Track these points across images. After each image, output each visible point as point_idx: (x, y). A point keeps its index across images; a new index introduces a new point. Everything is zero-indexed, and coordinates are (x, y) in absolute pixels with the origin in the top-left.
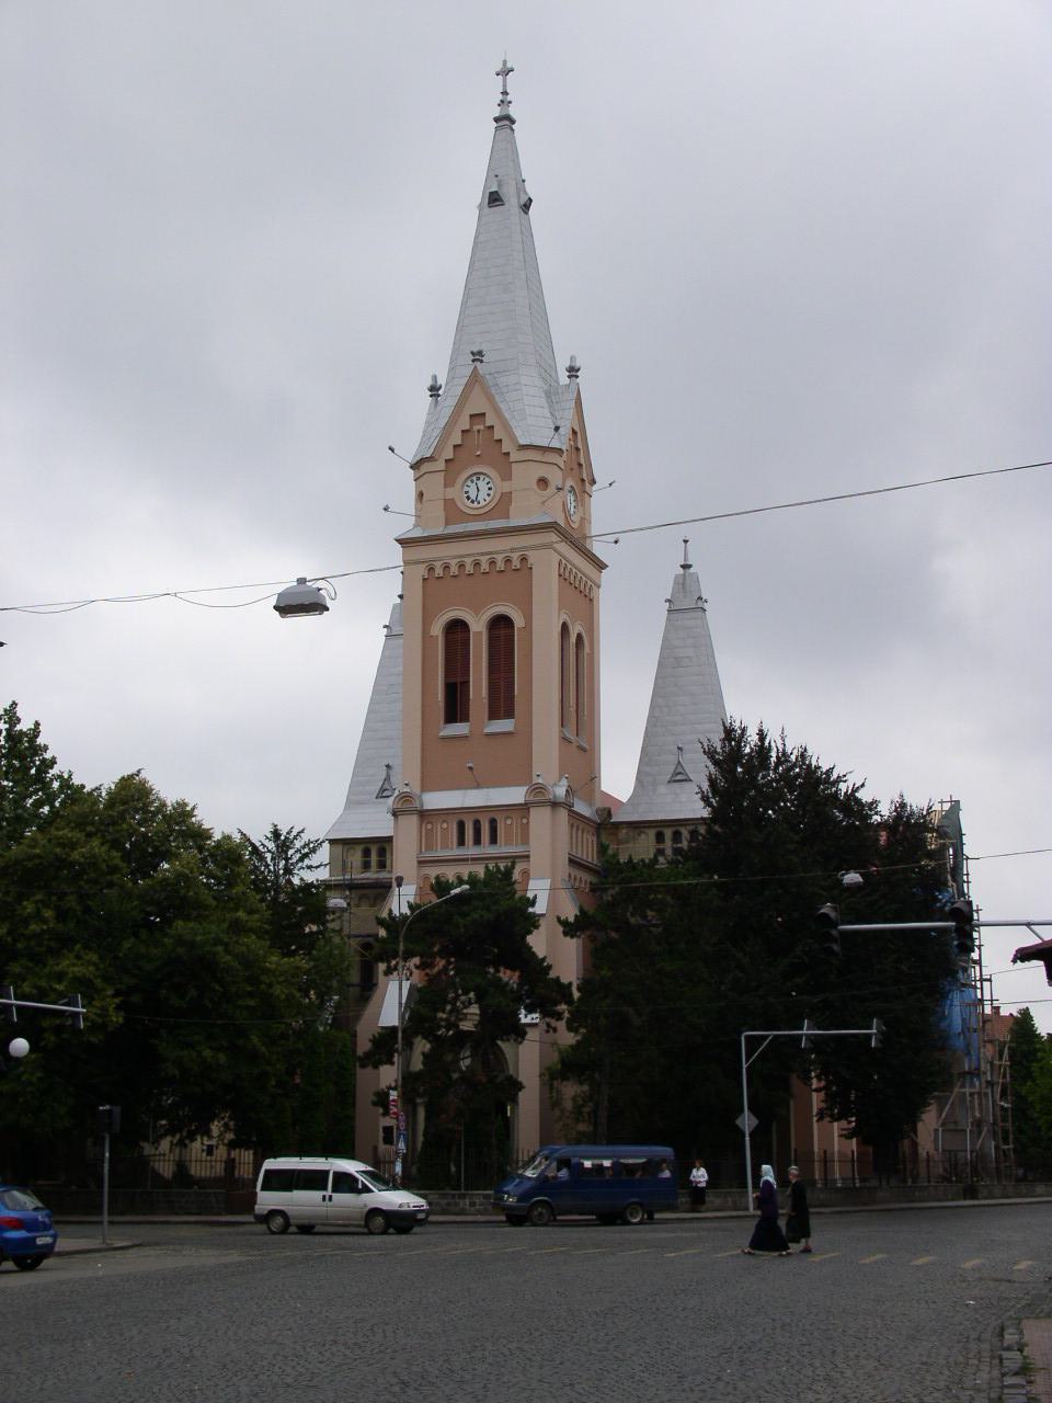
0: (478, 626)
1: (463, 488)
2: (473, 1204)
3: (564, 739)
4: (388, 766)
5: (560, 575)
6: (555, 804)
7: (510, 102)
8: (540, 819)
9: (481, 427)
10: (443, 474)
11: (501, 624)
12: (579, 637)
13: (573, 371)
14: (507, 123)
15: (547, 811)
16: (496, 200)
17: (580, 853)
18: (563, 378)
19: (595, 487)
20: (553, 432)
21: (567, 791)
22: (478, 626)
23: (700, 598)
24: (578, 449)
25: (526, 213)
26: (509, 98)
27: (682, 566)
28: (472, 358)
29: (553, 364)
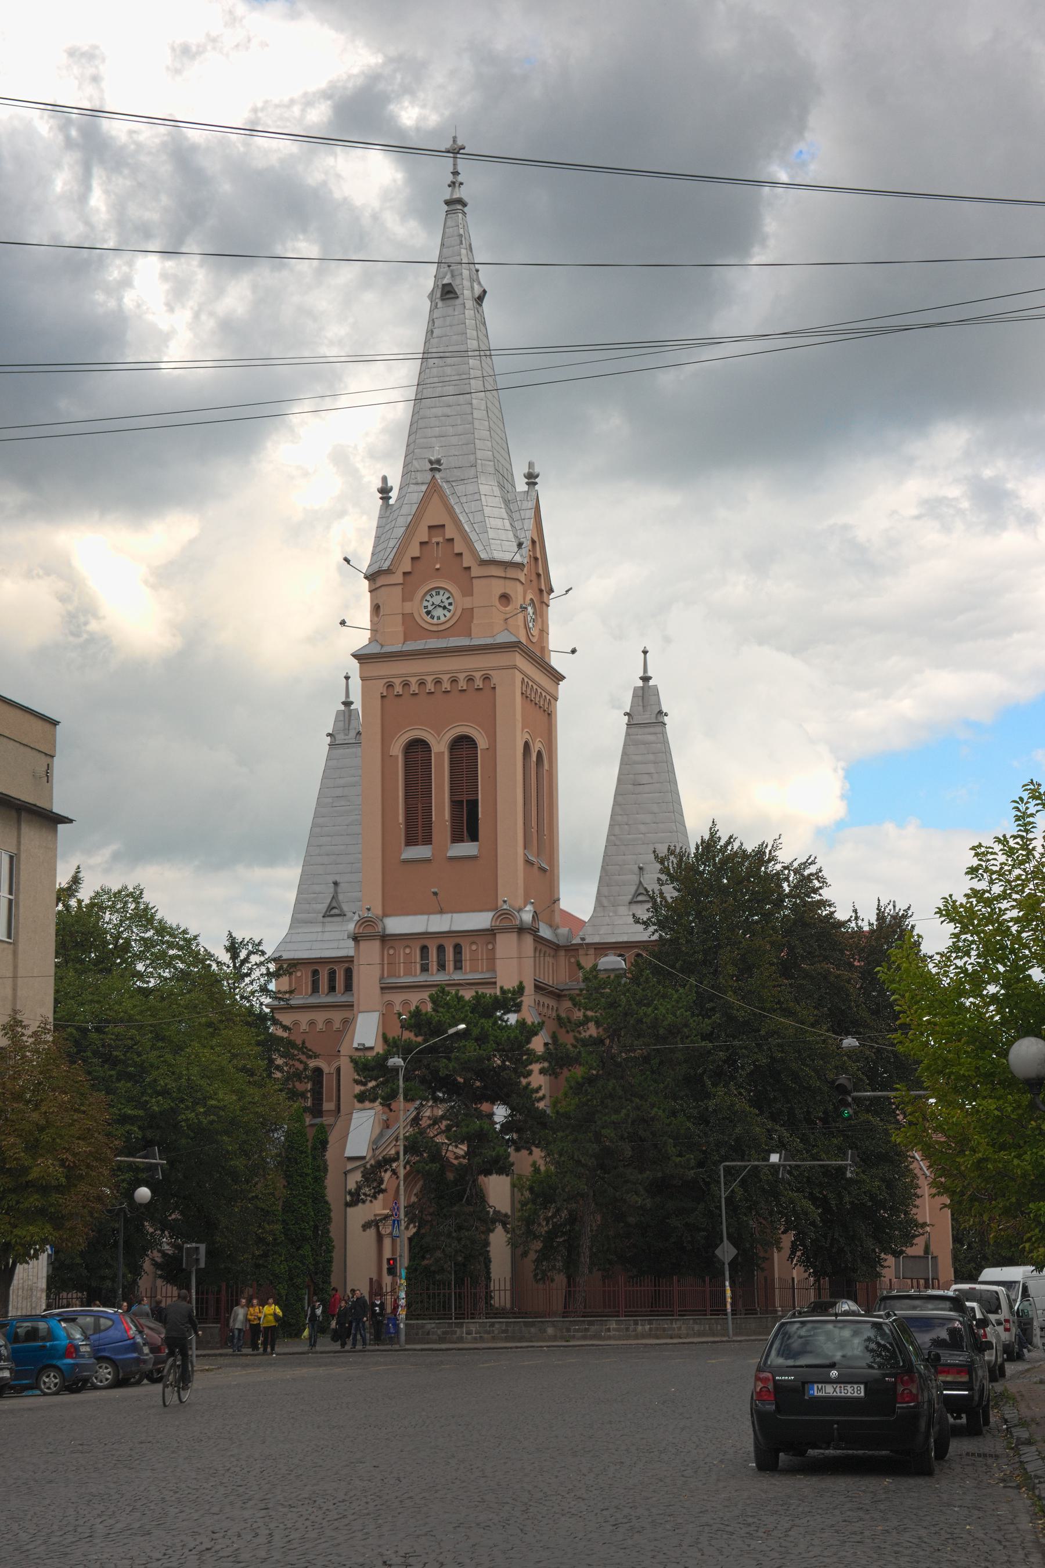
0: (440, 747)
1: (422, 600)
2: (469, 1333)
3: (528, 862)
4: (336, 884)
5: (522, 693)
6: (522, 930)
7: (461, 184)
8: (506, 945)
9: (440, 539)
10: (400, 587)
11: (463, 745)
12: (539, 753)
13: (532, 478)
14: (459, 207)
15: (513, 937)
16: (449, 292)
17: (542, 977)
18: (521, 486)
19: (552, 596)
20: (516, 549)
21: (533, 917)
22: (440, 747)
23: (660, 712)
24: (536, 559)
25: (481, 305)
26: (460, 178)
27: (641, 678)
28: (430, 466)
29: (509, 469)
